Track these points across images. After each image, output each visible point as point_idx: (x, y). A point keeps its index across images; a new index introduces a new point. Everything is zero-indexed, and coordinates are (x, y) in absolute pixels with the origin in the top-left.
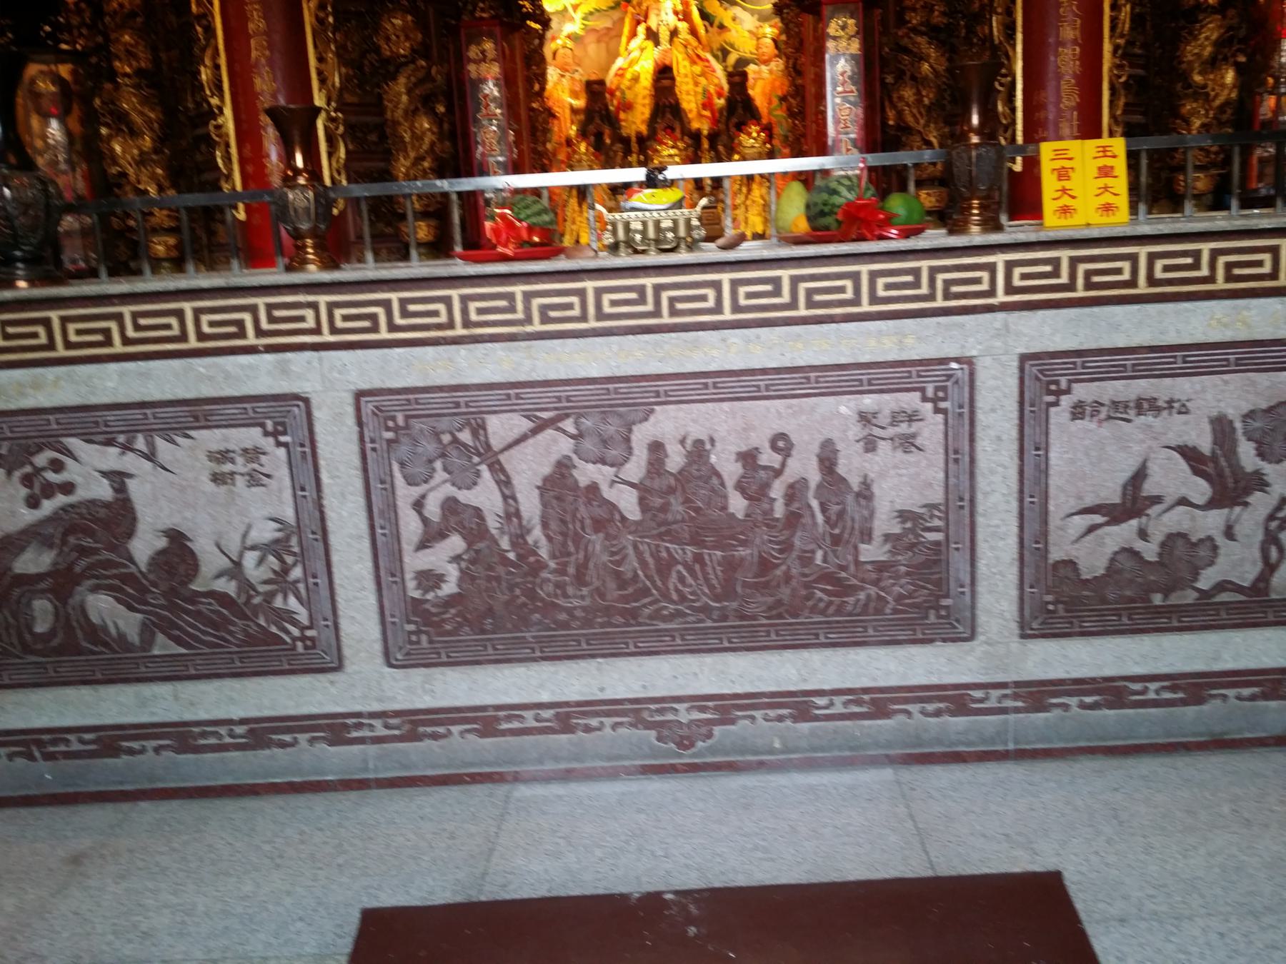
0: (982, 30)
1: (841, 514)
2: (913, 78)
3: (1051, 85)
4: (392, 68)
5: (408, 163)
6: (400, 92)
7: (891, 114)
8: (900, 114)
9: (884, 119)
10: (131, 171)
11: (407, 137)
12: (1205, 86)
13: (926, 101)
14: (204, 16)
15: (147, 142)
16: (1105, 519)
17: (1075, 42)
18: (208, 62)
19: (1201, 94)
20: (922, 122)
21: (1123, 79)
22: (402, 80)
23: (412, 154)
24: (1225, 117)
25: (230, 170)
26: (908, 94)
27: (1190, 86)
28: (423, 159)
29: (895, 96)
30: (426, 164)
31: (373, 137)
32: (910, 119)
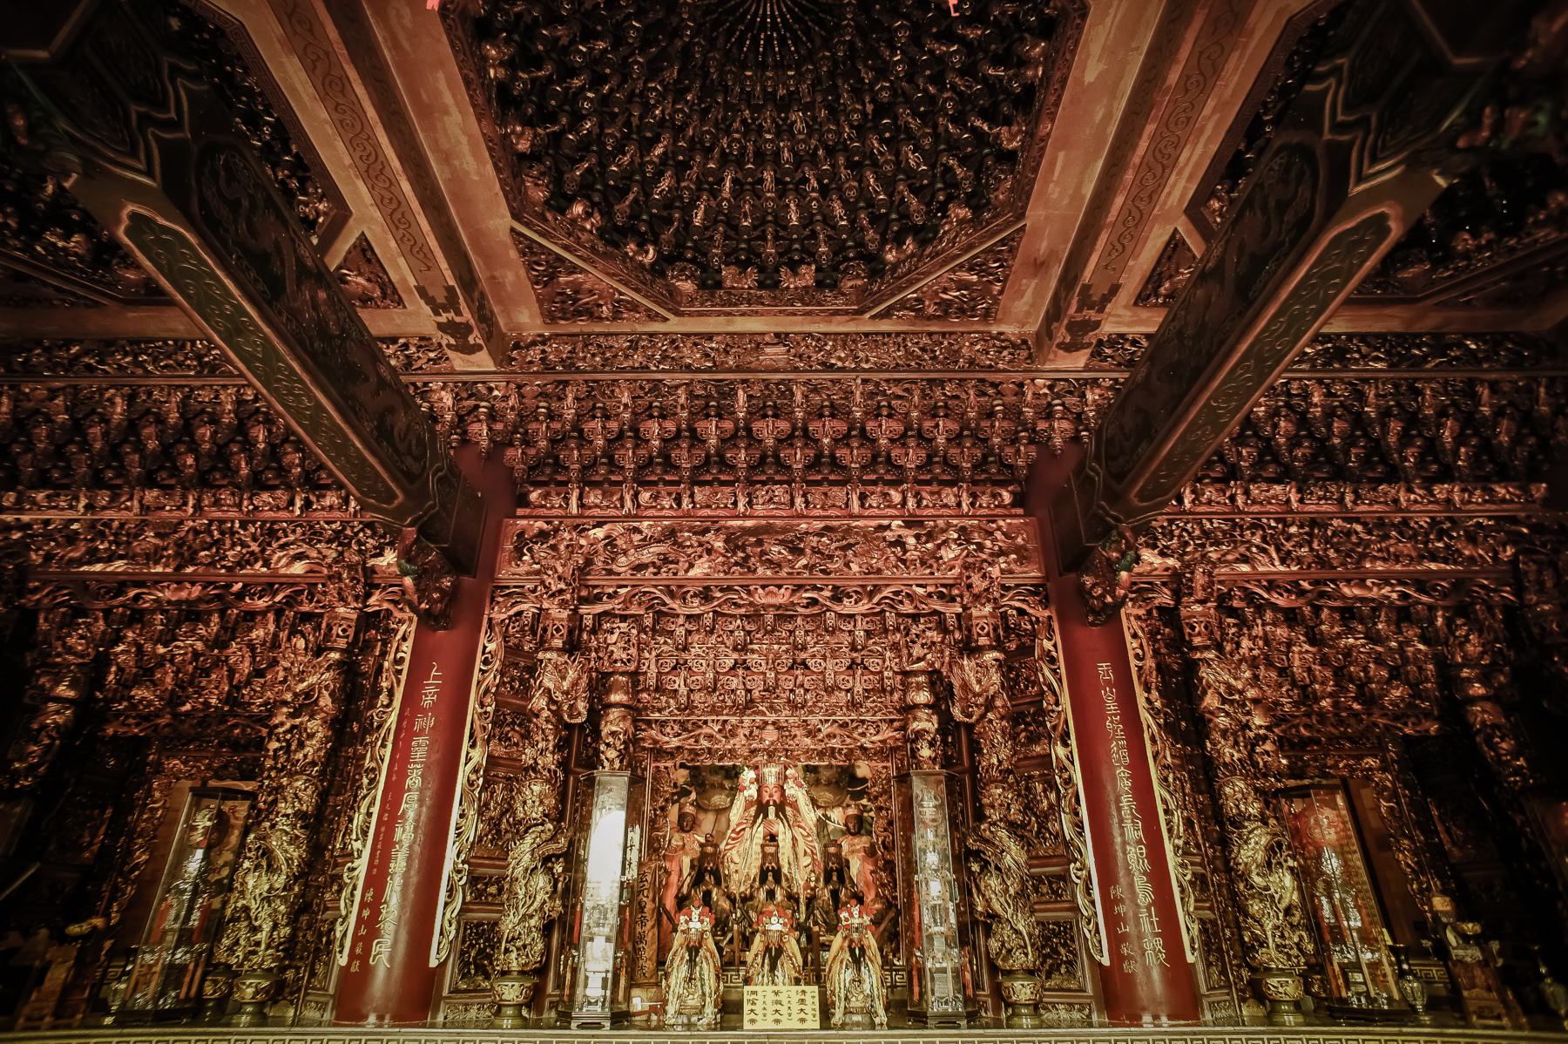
0: (1053, 826)
1: (624, 262)
2: (997, 868)
3: (1123, 880)
4: (522, 829)
5: (516, 920)
6: (523, 852)
7: (978, 900)
8: (988, 902)
9: (972, 906)
10: (254, 906)
11: (521, 893)
12: (1267, 888)
13: (1012, 891)
14: (373, 770)
15: (280, 881)
16: (1105, 101)
17: (1139, 842)
18: (363, 810)
19: (1263, 895)
20: (1010, 911)
21: (1188, 877)
22: (529, 839)
23: (522, 911)
24: (1295, 920)
25: (349, 913)
26: (994, 882)
27: (1252, 887)
28: (531, 916)
29: (982, 885)
30: (533, 922)
31: (493, 890)
32: (997, 907)
